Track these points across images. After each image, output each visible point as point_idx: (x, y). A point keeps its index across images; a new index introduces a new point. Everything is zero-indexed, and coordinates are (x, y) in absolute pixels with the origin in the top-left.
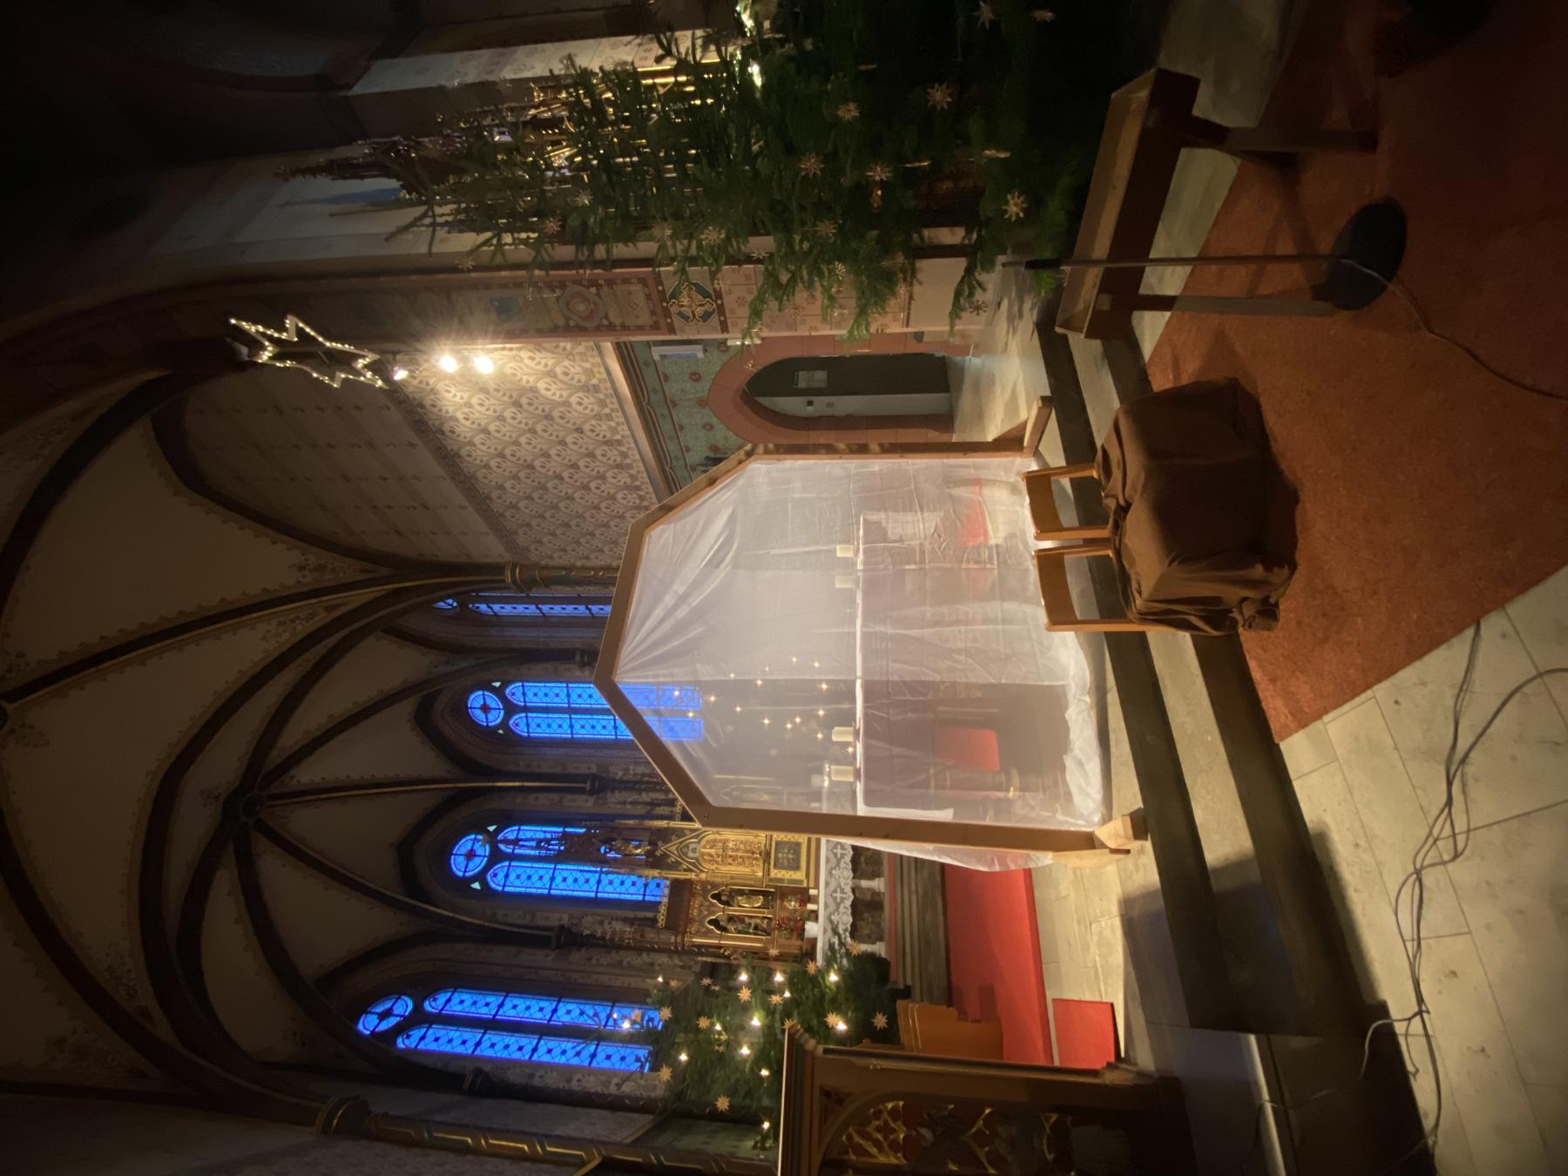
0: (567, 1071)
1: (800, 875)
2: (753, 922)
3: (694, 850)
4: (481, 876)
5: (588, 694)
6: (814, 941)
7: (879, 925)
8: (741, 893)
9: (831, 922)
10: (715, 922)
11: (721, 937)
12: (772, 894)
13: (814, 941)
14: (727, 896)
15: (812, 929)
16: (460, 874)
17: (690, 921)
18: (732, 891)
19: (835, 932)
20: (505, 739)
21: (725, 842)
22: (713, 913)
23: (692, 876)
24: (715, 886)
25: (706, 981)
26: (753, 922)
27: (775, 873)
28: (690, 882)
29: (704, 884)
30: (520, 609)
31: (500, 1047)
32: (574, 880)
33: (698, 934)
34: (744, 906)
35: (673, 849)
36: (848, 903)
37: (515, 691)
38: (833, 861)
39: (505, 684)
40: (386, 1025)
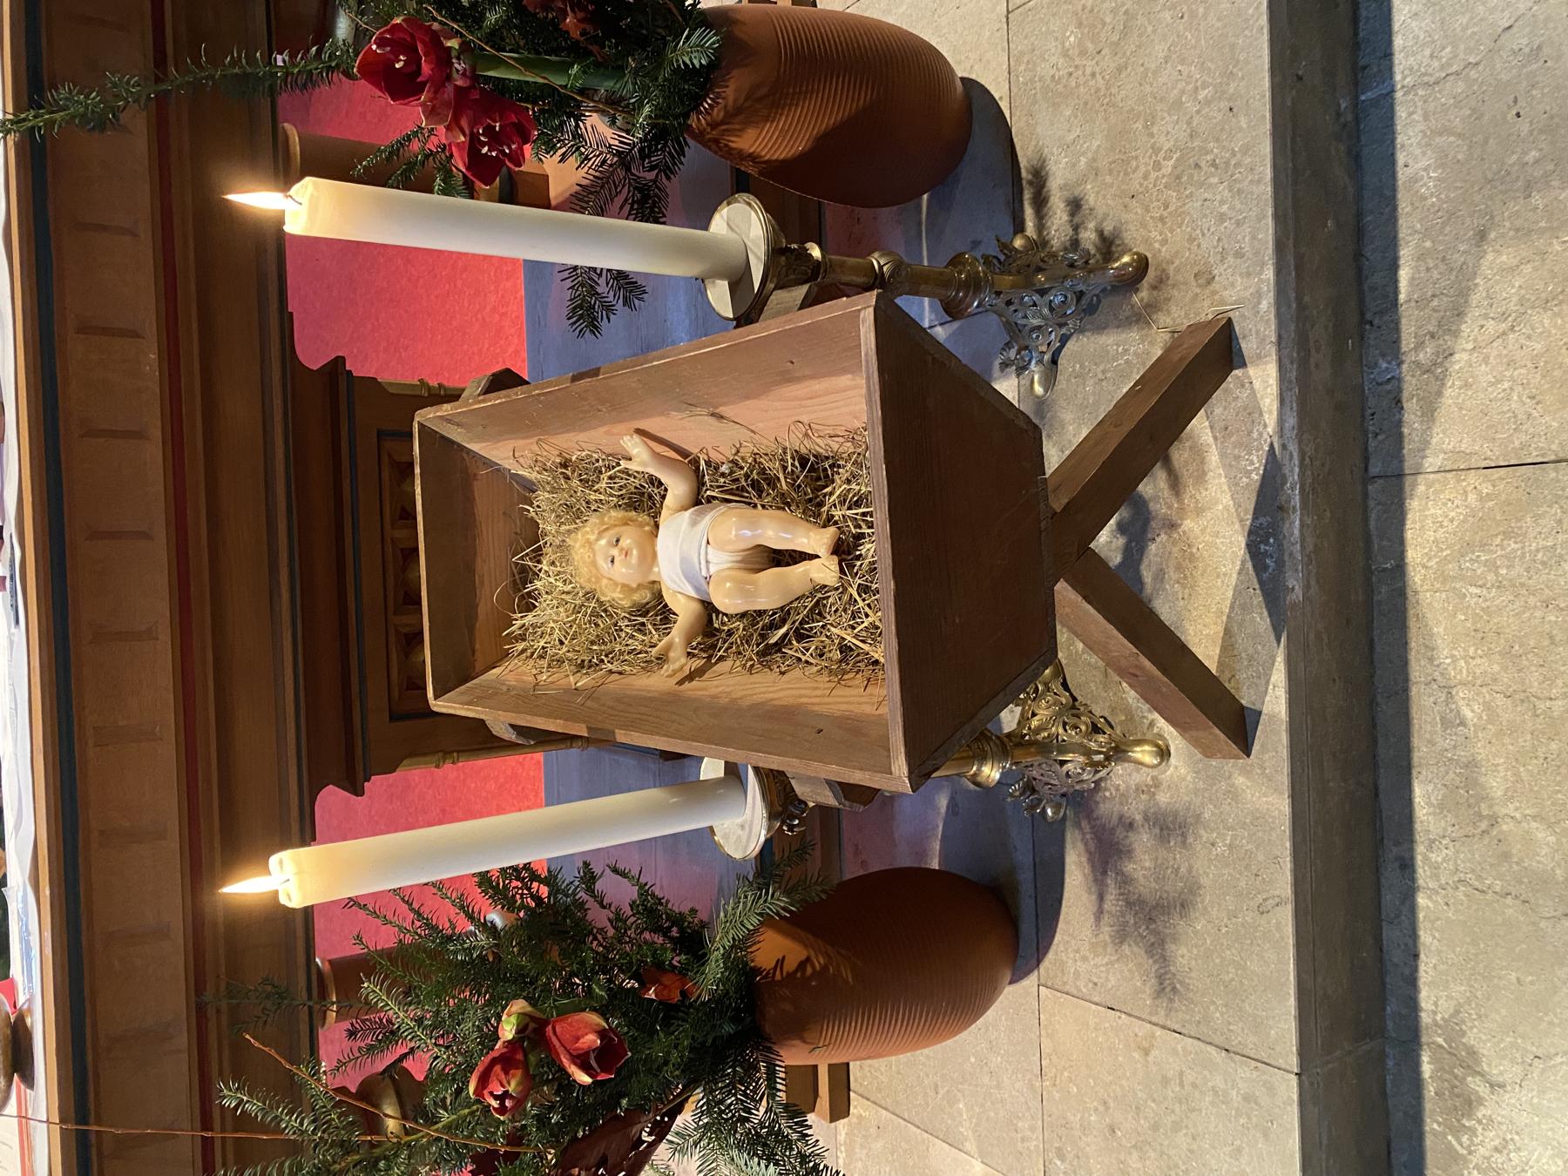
20: (740, 151)
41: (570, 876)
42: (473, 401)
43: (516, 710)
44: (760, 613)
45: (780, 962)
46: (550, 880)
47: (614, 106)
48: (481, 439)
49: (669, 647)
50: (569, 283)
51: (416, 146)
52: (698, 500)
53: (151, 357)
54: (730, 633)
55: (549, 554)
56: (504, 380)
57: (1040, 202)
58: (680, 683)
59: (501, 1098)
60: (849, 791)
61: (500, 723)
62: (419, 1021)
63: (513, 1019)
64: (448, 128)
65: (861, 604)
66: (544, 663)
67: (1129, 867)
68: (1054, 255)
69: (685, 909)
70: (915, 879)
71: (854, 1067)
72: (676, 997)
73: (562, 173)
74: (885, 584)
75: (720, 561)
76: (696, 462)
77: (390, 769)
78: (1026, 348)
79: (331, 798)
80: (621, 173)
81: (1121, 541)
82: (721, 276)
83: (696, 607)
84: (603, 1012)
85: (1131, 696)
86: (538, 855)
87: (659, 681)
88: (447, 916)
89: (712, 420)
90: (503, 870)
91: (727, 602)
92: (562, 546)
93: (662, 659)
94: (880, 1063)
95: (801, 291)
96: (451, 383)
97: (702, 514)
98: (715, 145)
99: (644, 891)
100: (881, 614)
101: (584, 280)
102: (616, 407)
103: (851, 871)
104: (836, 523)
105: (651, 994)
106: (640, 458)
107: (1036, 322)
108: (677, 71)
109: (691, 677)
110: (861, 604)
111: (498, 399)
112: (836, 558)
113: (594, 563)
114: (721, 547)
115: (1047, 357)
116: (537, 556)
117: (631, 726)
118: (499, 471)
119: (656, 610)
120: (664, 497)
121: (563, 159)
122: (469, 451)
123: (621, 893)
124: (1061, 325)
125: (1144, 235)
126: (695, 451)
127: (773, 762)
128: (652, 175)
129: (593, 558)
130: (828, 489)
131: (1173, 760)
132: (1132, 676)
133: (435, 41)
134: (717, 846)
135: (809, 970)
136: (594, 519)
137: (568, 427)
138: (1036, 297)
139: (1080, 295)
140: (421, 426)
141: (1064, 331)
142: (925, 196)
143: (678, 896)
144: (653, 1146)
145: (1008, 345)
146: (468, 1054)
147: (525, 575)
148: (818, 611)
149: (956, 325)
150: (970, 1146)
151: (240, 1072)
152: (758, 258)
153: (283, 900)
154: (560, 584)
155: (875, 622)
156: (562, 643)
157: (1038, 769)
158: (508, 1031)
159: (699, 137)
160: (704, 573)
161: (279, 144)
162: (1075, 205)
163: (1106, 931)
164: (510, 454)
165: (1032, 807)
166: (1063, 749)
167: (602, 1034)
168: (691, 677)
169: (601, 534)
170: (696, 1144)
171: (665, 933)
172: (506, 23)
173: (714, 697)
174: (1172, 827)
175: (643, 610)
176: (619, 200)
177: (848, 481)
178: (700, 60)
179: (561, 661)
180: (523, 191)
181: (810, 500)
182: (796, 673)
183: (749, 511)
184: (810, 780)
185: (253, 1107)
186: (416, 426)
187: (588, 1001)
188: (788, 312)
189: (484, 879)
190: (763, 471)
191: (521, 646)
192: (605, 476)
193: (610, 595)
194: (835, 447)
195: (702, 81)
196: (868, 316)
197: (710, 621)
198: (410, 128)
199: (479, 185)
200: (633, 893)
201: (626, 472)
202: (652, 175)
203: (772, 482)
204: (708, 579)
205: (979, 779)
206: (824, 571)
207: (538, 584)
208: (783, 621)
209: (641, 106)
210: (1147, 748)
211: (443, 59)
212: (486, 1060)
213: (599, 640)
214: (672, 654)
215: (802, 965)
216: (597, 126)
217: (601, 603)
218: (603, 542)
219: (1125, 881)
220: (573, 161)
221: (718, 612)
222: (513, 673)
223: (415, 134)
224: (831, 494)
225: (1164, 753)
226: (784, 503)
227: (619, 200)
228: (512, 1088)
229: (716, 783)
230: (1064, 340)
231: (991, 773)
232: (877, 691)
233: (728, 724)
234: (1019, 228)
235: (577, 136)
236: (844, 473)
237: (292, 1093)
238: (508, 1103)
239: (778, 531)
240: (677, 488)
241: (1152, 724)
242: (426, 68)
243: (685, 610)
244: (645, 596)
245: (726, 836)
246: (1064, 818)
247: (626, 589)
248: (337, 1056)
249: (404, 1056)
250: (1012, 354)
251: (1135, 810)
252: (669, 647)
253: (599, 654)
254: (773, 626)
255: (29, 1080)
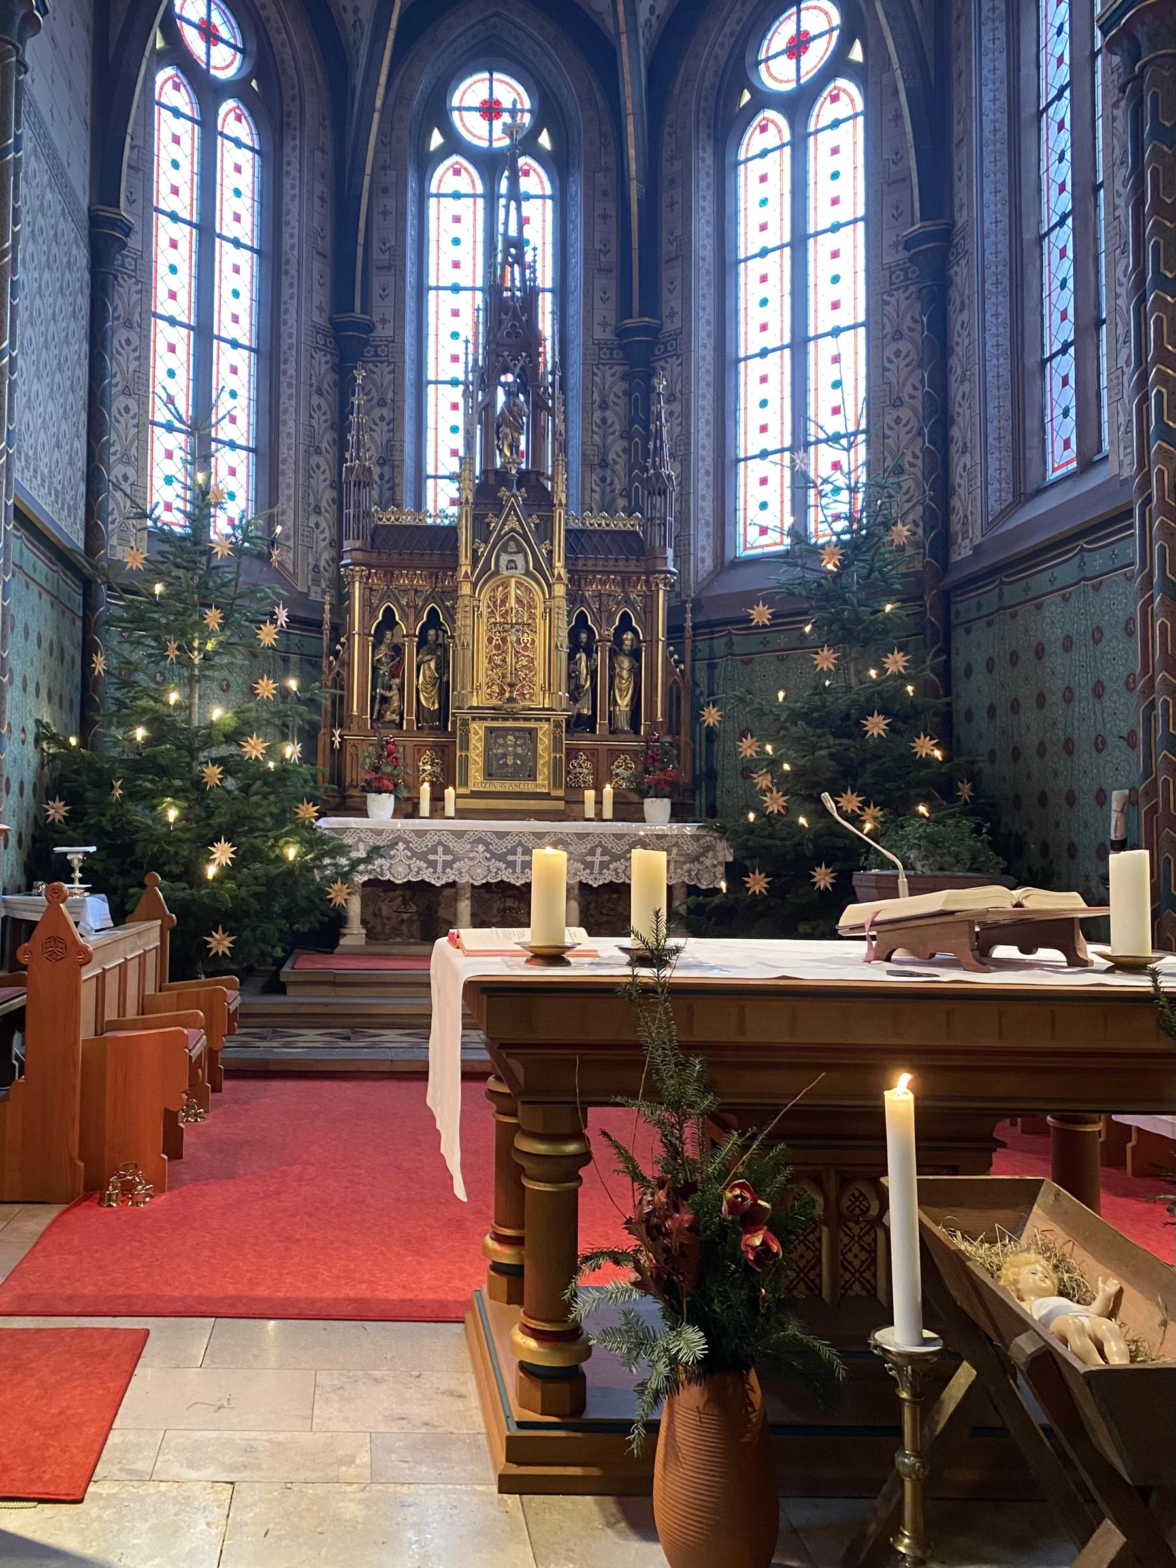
0: (139, 385)
1: (476, 779)
2: (394, 694)
3: (512, 565)
4: (455, 144)
5: (813, 45)
6: (362, 812)
7: (397, 932)
8: (442, 667)
9: (393, 845)
10: (389, 621)
11: (364, 635)
12: (441, 722)
13: (362, 812)
14: (436, 638)
15: (382, 806)
16: (455, 102)
17: (389, 574)
18: (446, 649)
19: (375, 852)
21: (530, 627)
22: (405, 617)
23: (465, 567)
24: (451, 614)
25: (282, 615)
26: (394, 694)
27: (477, 730)
28: (455, 567)
29: (453, 593)
30: (1060, 46)
31: (171, 252)
32: (451, 331)
33: (368, 590)
34: (420, 677)
35: (513, 523)
36: (427, 876)
37: (846, 100)
38: (502, 846)
39: (857, 73)
40: (193, 40)
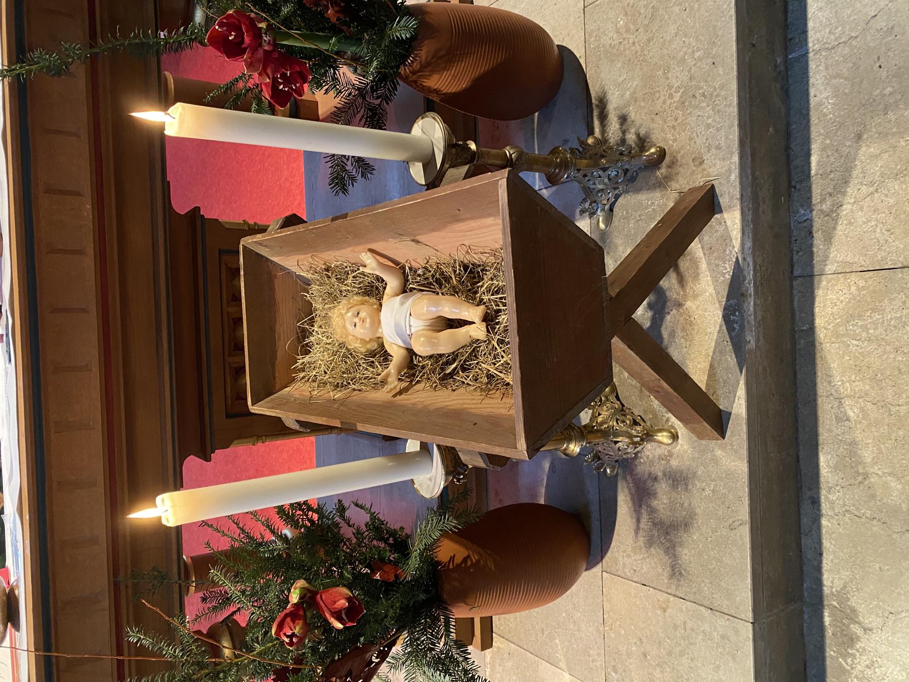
41: (330, 508)
42: (274, 232)
43: (299, 411)
44: (441, 356)
45: (452, 558)
46: (319, 510)
47: (356, 62)
48: (279, 254)
49: (388, 375)
50: (330, 164)
51: (241, 84)
52: (404, 290)
53: (88, 207)
54: (423, 367)
55: (318, 321)
56: (292, 221)
57: (603, 117)
58: (394, 396)
59: (290, 637)
60: (492, 459)
61: (290, 419)
62: (243, 592)
63: (298, 591)
64: (260, 74)
65: (499, 350)
66: (316, 384)
67: (655, 503)
68: (611, 148)
69: (397, 527)
70: (530, 510)
71: (495, 619)
72: (392, 578)
73: (326, 101)
74: (513, 339)
75: (417, 325)
76: (403, 268)
77: (226, 446)
78: (595, 202)
79: (192, 463)
80: (360, 100)
81: (650, 314)
82: (418, 160)
83: (403, 352)
84: (350, 587)
85: (656, 403)
86: (312, 496)
87: (382, 395)
88: (259, 531)
89: (413, 244)
90: (292, 505)
91: (421, 349)
92: (326, 317)
93: (384, 382)
94: (510, 617)
95: (464, 169)
96: (262, 222)
97: (407, 298)
98: (415, 84)
99: (373, 517)
100: (511, 356)
101: (339, 163)
102: (357, 236)
103: (493, 505)
104: (485, 303)
105: (378, 577)
106: (371, 266)
107: (600, 187)
108: (392, 41)
109: (400, 393)
110: (499, 350)
111: (288, 231)
112: (484, 324)
113: (344, 327)
114: (418, 317)
115: (607, 207)
116: (312, 322)
117: (366, 421)
118: (289, 273)
119: (380, 354)
120: (385, 288)
121: (326, 92)
122: (272, 262)
123: (360, 518)
124: (615, 189)
125: (663, 136)
126: (403, 261)
127: (448, 442)
128: (378, 102)
129: (344, 324)
130: (480, 284)
131: (680, 441)
132: (656, 392)
133: (252, 24)
134: (416, 490)
135: (469, 563)
136: (344, 301)
137: (329, 248)
138: (600, 173)
139: (626, 171)
140: (244, 247)
141: (617, 192)
142: (536, 114)
143: (393, 519)
144: (378, 665)
145: (584, 200)
146: (271, 611)
147: (304, 334)
148: (474, 354)
149: (554, 188)
150: (562, 664)
151: (139, 622)
152: (439, 149)
153: (164, 522)
154: (324, 339)
155: (507, 361)
156: (326, 373)
157: (602, 446)
158: (294, 598)
159: (405, 79)
160: (408, 332)
161: (162, 84)
162: (623, 119)
163: (641, 540)
164: (296, 263)
165: (598, 468)
166: (616, 434)
167: (349, 599)
168: (400, 393)
169: (348, 310)
170: (403, 663)
171: (386, 541)
172: (293, 13)
173: (414, 404)
174: (679, 480)
175: (373, 354)
176: (359, 116)
177: (492, 279)
178: (406, 35)
179: (325, 384)
180: (303, 111)
181: (470, 290)
182: (462, 390)
183: (434, 296)
184: (469, 452)
185: (147, 642)
186: (241, 247)
187: (341, 581)
188: (457, 181)
189: (281, 510)
190: (442, 273)
191: (302, 375)
192: (350, 276)
193: (354, 345)
194: (484, 259)
195: (407, 47)
196: (503, 183)
197: (412, 360)
198: (238, 74)
199: (278, 107)
200: (367, 518)
201: (363, 274)
202: (378, 102)
203: (448, 279)
204: (410, 336)
205: (568, 452)
206: (478, 331)
207: (312, 339)
208: (454, 360)
209: (372, 61)
210: (665, 434)
211: (257, 34)
212: (282, 615)
213: (347, 371)
214: (389, 380)
215: (465, 560)
216: (346, 73)
217: (348, 350)
218: (350, 314)
219: (652, 511)
220: (332, 93)
221: (416, 355)
222: (297, 390)
223: (241, 78)
224: (482, 286)
225: (675, 437)
226: (455, 292)
227: (359, 116)
228: (297, 631)
229: (415, 454)
230: (617, 197)
231: (574, 448)
232: (508, 401)
233: (422, 420)
234: (591, 132)
235: (335, 79)
236: (489, 275)
237: (169, 634)
238: (294, 640)
239: (451, 308)
240: (392, 283)
241: (668, 420)
242: (247, 40)
243: (397, 354)
244: (374, 346)
245: (421, 485)
246: (617, 474)
247: (363, 341)
248: (196, 613)
249: (234, 612)
250: (587, 205)
251: (658, 470)
252: (388, 375)
253: (347, 379)
254: (448, 363)
255: (17, 626)
